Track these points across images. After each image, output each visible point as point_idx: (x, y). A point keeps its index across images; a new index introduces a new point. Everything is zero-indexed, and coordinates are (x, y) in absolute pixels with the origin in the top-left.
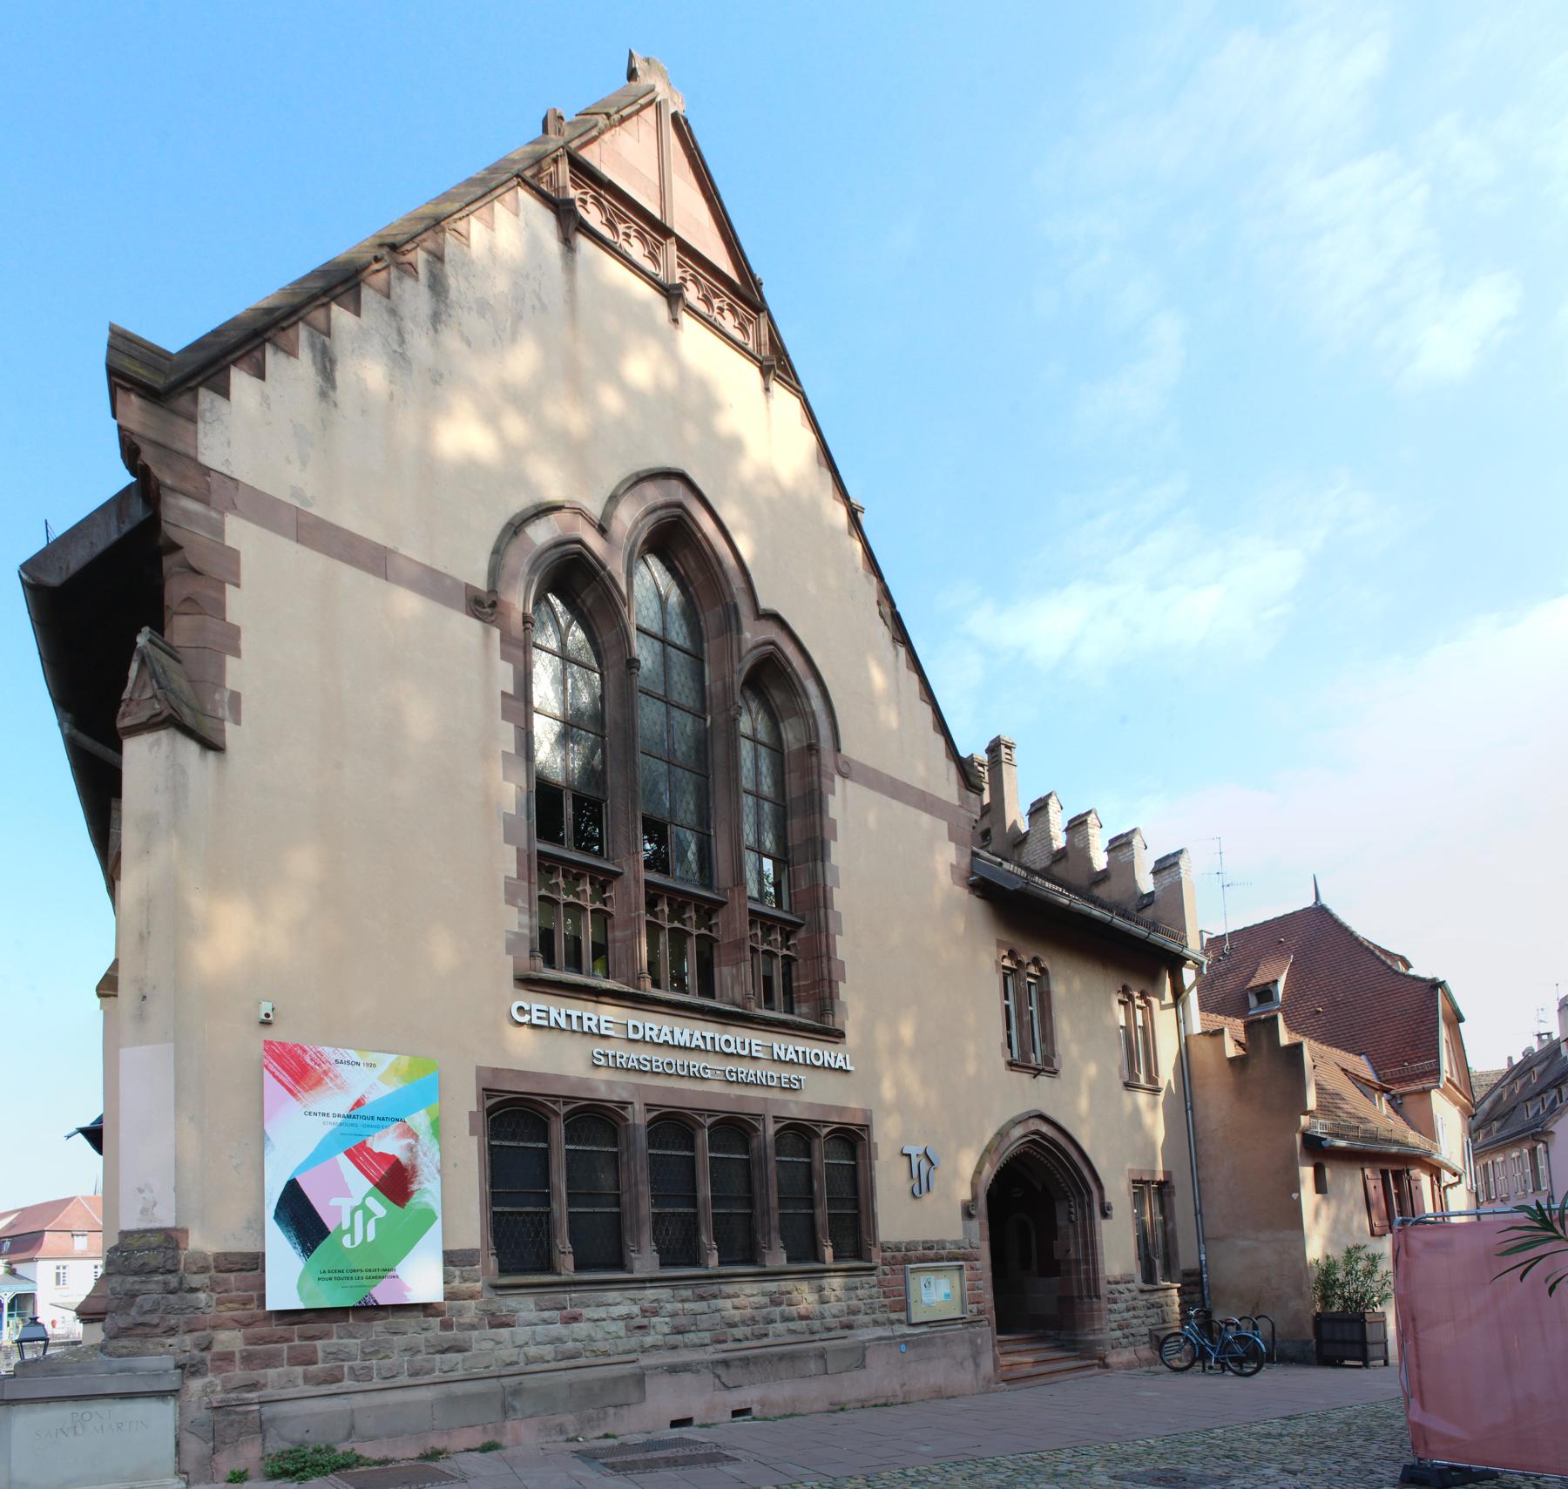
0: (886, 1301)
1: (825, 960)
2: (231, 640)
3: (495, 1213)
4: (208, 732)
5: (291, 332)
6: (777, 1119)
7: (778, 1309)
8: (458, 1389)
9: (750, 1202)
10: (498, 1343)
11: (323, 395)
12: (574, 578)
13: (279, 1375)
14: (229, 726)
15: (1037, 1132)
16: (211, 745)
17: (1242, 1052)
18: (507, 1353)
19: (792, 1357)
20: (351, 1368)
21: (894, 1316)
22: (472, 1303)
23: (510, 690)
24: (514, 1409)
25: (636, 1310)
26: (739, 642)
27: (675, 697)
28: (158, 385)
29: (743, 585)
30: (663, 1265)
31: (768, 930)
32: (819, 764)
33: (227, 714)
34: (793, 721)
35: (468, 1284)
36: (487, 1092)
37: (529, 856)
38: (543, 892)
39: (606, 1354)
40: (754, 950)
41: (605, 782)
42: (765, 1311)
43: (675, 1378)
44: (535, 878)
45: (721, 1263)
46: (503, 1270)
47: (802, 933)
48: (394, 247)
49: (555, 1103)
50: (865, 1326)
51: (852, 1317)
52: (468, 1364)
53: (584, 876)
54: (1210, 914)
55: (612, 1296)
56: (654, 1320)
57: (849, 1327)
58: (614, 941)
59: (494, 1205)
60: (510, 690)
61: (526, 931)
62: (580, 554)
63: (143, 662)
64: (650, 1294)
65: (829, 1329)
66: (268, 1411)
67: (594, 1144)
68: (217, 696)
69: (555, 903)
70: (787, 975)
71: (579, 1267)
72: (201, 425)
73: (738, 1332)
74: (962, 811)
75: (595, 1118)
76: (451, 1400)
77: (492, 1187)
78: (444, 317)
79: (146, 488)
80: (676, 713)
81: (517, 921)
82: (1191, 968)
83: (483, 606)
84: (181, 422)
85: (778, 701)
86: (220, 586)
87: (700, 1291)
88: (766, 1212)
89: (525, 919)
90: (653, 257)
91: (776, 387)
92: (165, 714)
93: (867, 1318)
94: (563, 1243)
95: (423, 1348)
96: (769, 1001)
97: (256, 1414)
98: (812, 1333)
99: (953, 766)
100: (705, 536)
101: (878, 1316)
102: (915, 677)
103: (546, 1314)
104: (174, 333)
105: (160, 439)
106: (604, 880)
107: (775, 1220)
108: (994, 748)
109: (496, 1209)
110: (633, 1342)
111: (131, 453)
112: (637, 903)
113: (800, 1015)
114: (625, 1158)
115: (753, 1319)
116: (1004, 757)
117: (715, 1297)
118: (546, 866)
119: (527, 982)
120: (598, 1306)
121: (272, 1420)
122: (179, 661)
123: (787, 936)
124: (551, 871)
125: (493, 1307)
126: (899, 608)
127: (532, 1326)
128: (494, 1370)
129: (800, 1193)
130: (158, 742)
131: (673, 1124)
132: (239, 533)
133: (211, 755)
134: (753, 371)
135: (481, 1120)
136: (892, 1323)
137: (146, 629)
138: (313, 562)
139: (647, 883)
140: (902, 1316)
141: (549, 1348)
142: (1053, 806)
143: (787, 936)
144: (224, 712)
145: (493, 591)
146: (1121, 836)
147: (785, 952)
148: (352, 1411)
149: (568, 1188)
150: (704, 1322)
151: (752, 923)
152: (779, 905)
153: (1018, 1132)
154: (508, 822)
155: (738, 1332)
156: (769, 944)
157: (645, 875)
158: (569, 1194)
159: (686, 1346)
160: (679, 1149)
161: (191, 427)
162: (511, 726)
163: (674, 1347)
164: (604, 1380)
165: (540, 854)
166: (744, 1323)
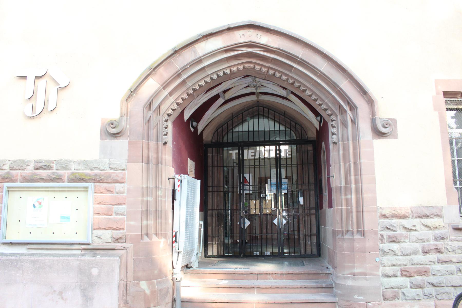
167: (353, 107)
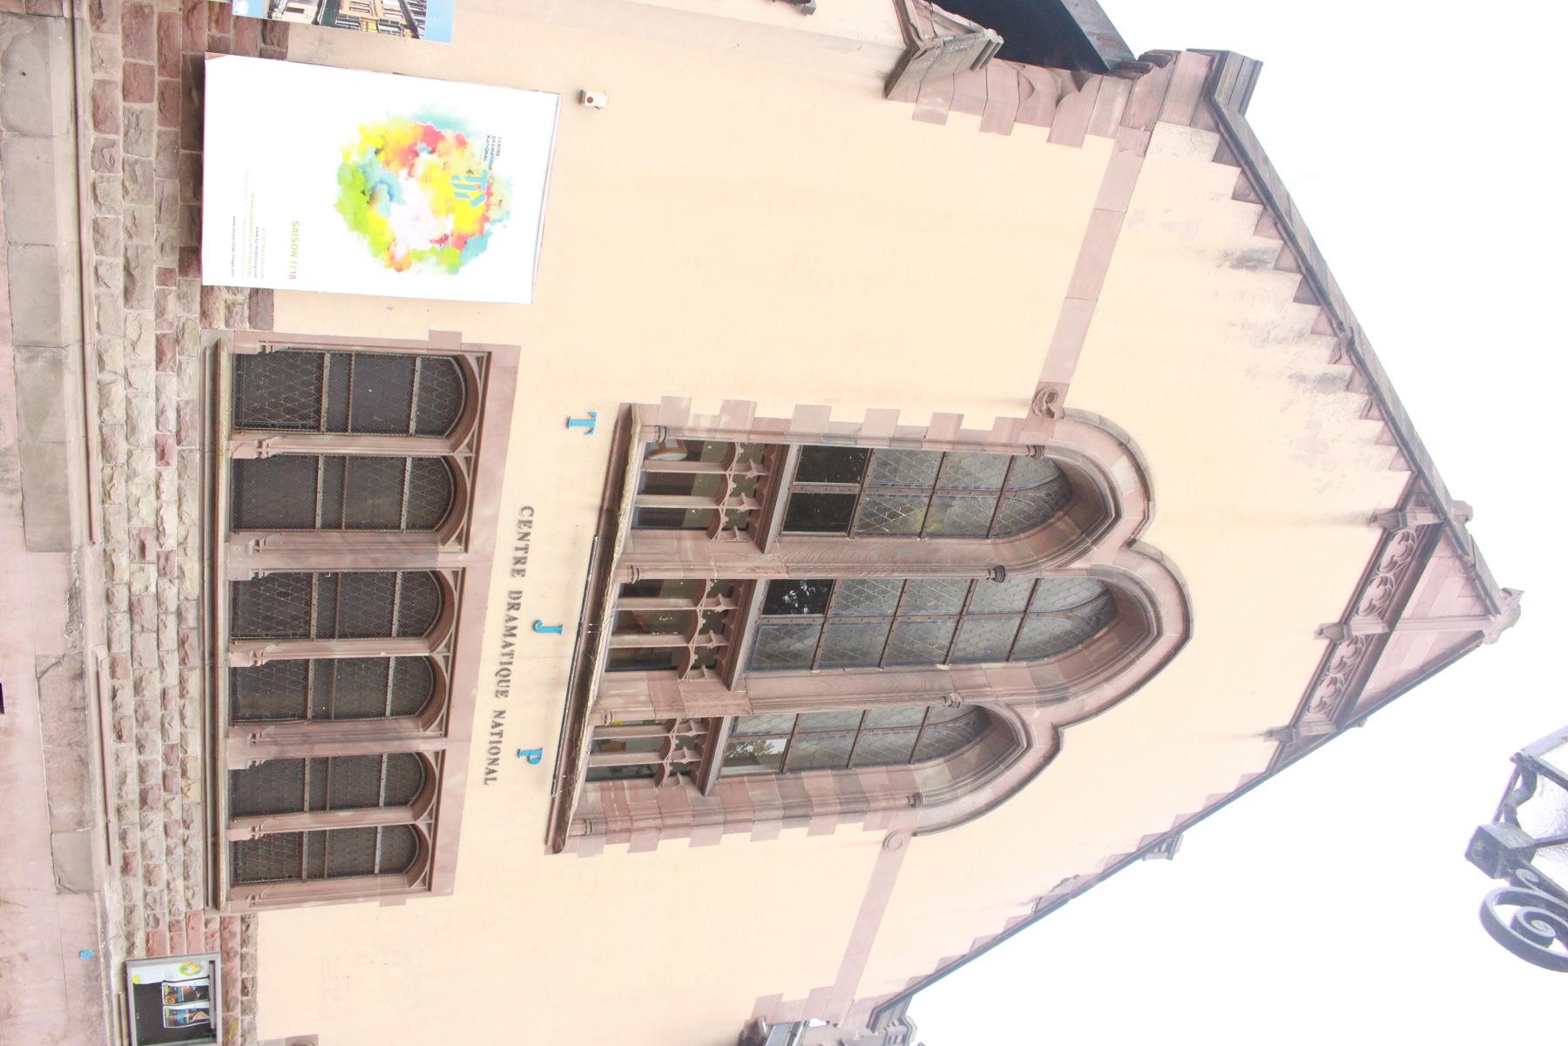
0: (164, 926)
1: (658, 822)
2: (995, 123)
3: (321, 356)
5: (1273, 232)
6: (441, 756)
7: (159, 757)
8: (69, 284)
9: (323, 717)
10: (134, 346)
11: (1227, 255)
13: (112, 50)
14: (910, 107)
16: (890, 83)
18: (117, 359)
19: (81, 778)
20: (113, 144)
22: (196, 314)
23: (965, 425)
24: (31, 359)
25: (170, 543)
26: (1028, 703)
27: (967, 625)
28: (1217, 94)
29: (1087, 709)
30: (235, 586)
32: (898, 808)
33: (924, 108)
34: (947, 775)
35: (222, 312)
36: (486, 359)
37: (782, 434)
38: (739, 451)
39: (106, 496)
40: (669, 725)
41: (870, 535)
42: (158, 737)
43: (61, 598)
44: (755, 439)
45: (234, 672)
46: (240, 360)
48: (1351, 343)
49: (470, 446)
50: (127, 893)
52: (105, 300)
53: (760, 503)
55: (193, 509)
57: (126, 868)
58: (679, 538)
59: (333, 355)
60: (965, 425)
61: (690, 424)
63: (970, 31)
64: (193, 567)
66: (59, 29)
67: (412, 496)
68: (940, 100)
69: (726, 465)
70: (638, 773)
71: (238, 466)
72: (1188, 130)
73: (127, 696)
74: (848, 1004)
75: (446, 500)
76: (52, 277)
77: (359, 355)
78: (1302, 386)
79: (1130, 68)
81: (704, 416)
83: (1047, 401)
84: (1189, 111)
85: (967, 755)
86: (1048, 122)
87: (193, 640)
88: (307, 740)
89: (705, 424)
90: (1371, 608)
92: (919, 43)
93: (137, 895)
94: (277, 445)
95: (135, 241)
96: (600, 746)
97: (56, 12)
99: (898, 988)
100: (1132, 662)
101: (140, 914)
102: (999, 929)
103: (171, 415)
104: (1263, 119)
105: (1172, 88)
106: (753, 529)
107: (295, 752)
109: (327, 358)
110: (120, 534)
111: (1159, 59)
112: (727, 569)
113: (584, 791)
114: (391, 538)
115: (146, 718)
117: (183, 662)
118: (770, 455)
119: (626, 422)
121: (45, 31)
122: (972, 67)
123: (687, 771)
124: (764, 461)
125: (188, 342)
126: (1072, 902)
127: (157, 392)
128: (92, 336)
129: (338, 784)
131: (434, 605)
132: (1098, 150)
133: (880, 84)
134: (1283, 719)
135: (448, 347)
136: (129, 936)
137: (1001, 41)
140: (140, 951)
141: (121, 415)
143: (687, 771)
144: (925, 105)
147: (668, 769)
148: (48, 137)
149: (354, 458)
150: (146, 643)
151: (703, 722)
154: (821, 411)
155: (127, 696)
156: (679, 748)
158: (343, 458)
159: (110, 617)
160: (402, 616)
161: (1186, 120)
162: (927, 424)
163: (108, 599)
164: (66, 492)
165: (784, 449)
166: (140, 705)
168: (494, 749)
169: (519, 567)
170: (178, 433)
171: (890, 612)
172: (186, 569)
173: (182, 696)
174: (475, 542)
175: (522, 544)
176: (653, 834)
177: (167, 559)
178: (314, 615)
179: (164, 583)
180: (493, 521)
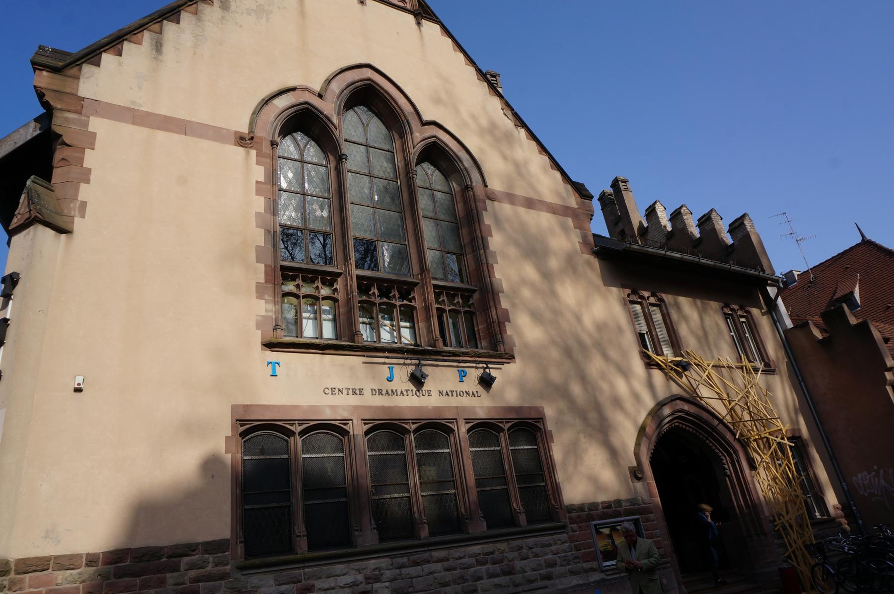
2: (85, 175)
4: (60, 222)
6: (467, 421)
12: (304, 121)
14: (77, 220)
15: (681, 411)
17: (827, 335)
21: (587, 565)
25: (360, 577)
31: (451, 297)
35: (219, 568)
36: (241, 421)
42: (472, 570)
47: (476, 296)
50: (562, 576)
51: (550, 570)
54: (789, 253)
56: (376, 585)
57: (548, 577)
60: (262, 179)
62: (307, 108)
64: (372, 564)
65: (531, 582)
68: (72, 205)
71: (311, 548)
72: (81, 80)
80: (376, 181)
82: (771, 285)
83: (244, 140)
86: (82, 150)
87: (415, 557)
91: (424, 22)
94: (300, 528)
98: (517, 586)
99: (569, 187)
101: (572, 566)
108: (615, 184)
115: (462, 577)
116: (622, 188)
117: (428, 562)
120: (328, 577)
123: (466, 299)
130: (28, 233)
132: (96, 124)
134: (411, 18)
136: (586, 571)
138: (140, 133)
139: (358, 277)
142: (659, 209)
145: (251, 132)
146: (704, 215)
152: (462, 281)
153: (667, 411)
157: (356, 272)
161: (76, 81)
166: (455, 582)
167: (736, 452)
168: (460, 394)
169: (358, 392)
170: (294, 583)
171: (372, 210)
172: (373, 567)
173: (448, 560)
174: (346, 415)
175: (345, 392)
176: (498, 310)
177: (369, 578)
178: (396, 495)
179: (384, 578)
180: (332, 407)
